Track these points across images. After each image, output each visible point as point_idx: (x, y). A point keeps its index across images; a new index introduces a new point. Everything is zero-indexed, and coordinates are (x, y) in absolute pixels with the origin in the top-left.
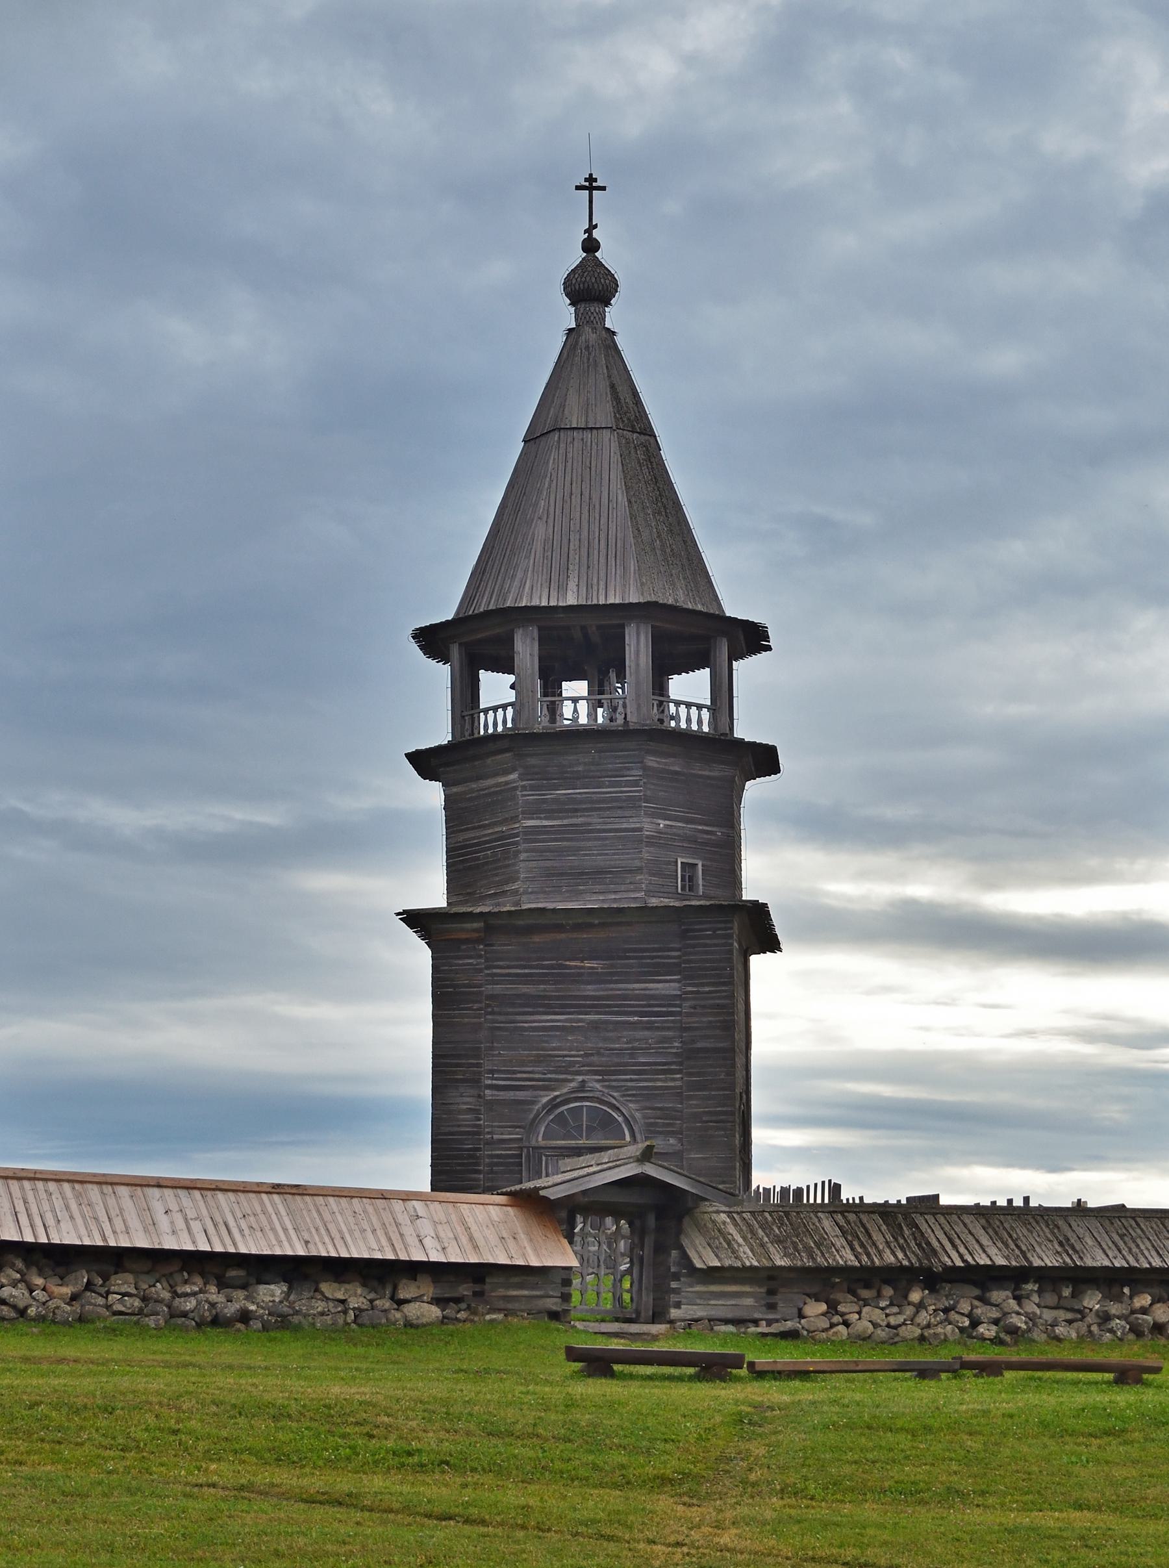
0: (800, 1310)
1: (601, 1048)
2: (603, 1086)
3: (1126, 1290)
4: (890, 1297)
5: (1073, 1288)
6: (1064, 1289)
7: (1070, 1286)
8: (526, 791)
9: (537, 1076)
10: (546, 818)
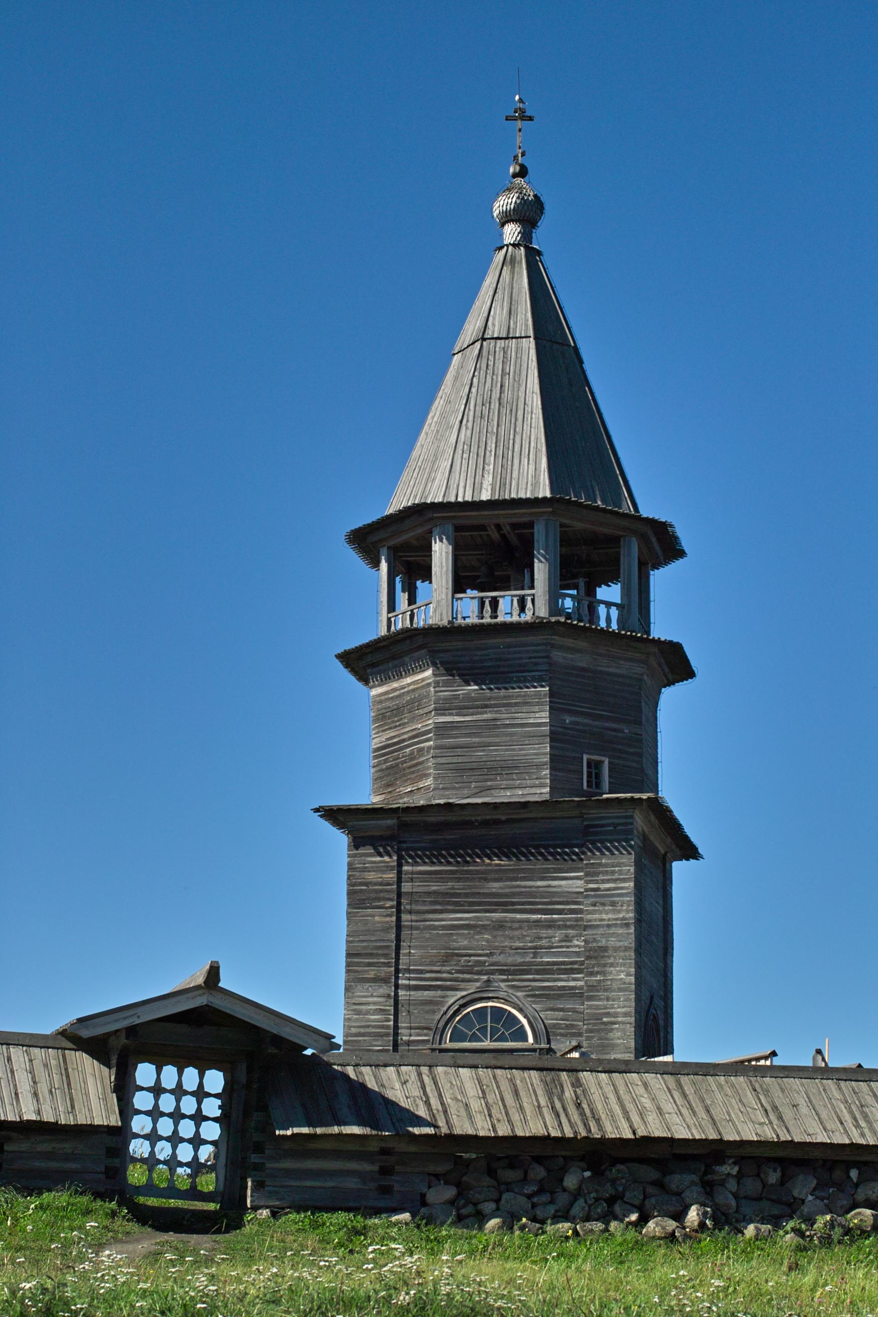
0: (423, 1196)
1: (506, 947)
2: (508, 986)
3: (854, 1174)
4: (541, 1181)
5: (782, 1172)
6: (771, 1172)
7: (779, 1170)
8: (439, 687)
9: (445, 975)
10: (458, 715)
